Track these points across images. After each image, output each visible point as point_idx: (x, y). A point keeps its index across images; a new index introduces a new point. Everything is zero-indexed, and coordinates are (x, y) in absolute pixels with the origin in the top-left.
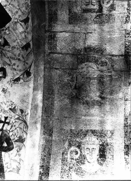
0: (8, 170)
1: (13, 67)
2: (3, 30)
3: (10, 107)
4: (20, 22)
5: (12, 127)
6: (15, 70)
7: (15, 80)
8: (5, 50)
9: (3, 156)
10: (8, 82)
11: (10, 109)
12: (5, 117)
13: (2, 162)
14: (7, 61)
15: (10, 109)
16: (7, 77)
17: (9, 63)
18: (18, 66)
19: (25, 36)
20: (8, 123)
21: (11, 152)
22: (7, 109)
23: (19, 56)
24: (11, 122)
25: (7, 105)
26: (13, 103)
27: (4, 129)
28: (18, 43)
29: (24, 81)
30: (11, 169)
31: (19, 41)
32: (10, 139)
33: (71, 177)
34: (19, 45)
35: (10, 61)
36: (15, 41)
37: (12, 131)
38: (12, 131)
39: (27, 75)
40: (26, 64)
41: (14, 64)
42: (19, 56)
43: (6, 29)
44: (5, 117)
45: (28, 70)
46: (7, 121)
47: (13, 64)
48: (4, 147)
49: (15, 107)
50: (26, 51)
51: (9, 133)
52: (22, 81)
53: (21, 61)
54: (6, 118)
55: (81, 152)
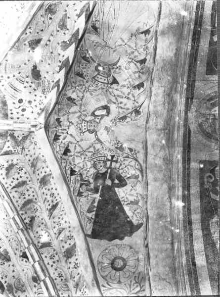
0: (126, 203)
1: (119, 105)
2: (113, 68)
3: (116, 146)
4: (136, 63)
5: (121, 165)
6: (122, 108)
7: (120, 119)
8: (113, 88)
9: (117, 192)
10: (111, 121)
11: (117, 148)
12: (111, 156)
13: (118, 196)
14: (113, 99)
15: (117, 148)
16: (110, 115)
17: (115, 101)
18: (125, 105)
19: (139, 76)
20: (116, 162)
21: (124, 188)
22: (113, 148)
23: (128, 95)
24: (119, 160)
25: (112, 143)
26: (119, 142)
27: (113, 167)
28: (130, 82)
29: (132, 120)
30: (129, 202)
31: (131, 80)
32: (121, 176)
33: (66, 228)
34: (130, 85)
35: (116, 99)
36: (125, 80)
37: (122, 169)
38: (122, 169)
39: (135, 113)
40: (135, 103)
41: (121, 103)
42: (128, 95)
43: (117, 68)
44: (111, 156)
45: (138, 109)
46: (114, 159)
47: (119, 102)
48: (115, 183)
49: (122, 146)
50: (137, 90)
51: (118, 171)
52: (128, 119)
53: (130, 99)
54: (113, 157)
55: (215, 177)
